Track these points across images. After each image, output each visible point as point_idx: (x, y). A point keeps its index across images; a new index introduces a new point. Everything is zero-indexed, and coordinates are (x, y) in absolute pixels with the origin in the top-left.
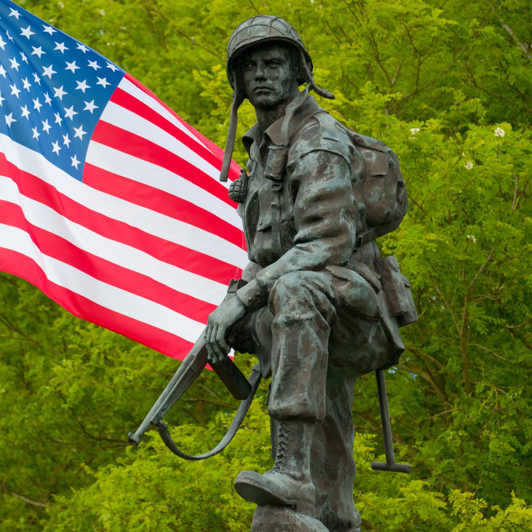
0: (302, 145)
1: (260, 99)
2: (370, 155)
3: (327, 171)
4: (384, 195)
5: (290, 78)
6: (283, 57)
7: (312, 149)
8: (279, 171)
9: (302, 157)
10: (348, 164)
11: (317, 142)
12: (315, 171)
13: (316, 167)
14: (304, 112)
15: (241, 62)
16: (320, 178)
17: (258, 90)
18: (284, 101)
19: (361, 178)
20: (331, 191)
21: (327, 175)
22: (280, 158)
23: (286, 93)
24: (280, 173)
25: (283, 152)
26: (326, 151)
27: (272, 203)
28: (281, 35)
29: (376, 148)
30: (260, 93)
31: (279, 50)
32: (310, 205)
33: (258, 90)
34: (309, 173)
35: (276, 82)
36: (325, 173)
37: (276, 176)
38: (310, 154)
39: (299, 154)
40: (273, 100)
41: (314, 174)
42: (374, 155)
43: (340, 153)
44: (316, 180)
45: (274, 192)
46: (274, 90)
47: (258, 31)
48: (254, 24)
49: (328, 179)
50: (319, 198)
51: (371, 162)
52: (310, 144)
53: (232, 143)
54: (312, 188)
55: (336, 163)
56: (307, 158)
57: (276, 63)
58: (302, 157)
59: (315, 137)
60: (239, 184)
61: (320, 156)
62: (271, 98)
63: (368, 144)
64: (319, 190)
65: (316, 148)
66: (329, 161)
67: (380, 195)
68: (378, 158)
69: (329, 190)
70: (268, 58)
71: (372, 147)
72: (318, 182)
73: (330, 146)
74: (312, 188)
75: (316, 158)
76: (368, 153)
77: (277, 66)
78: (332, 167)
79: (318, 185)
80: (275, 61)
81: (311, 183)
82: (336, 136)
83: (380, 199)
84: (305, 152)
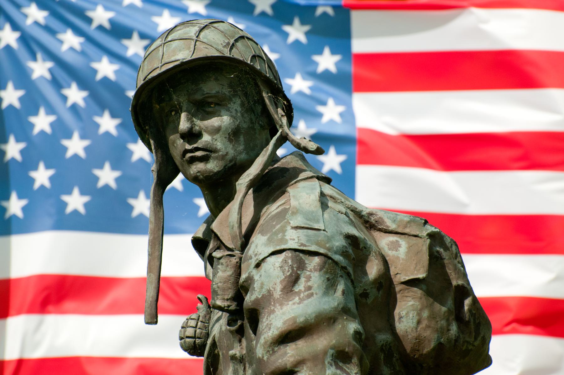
0: (259, 245)
1: (197, 168)
2: (395, 246)
3: (301, 286)
4: (426, 314)
5: (245, 126)
6: (226, 91)
7: (272, 250)
8: (230, 294)
9: (258, 266)
10: (344, 268)
11: (280, 236)
12: (279, 287)
13: (278, 281)
14: (275, 183)
15: (158, 105)
16: (288, 300)
17: (189, 155)
18: (236, 169)
19: (378, 290)
20: (306, 320)
21: (300, 291)
22: (230, 272)
23: (241, 153)
24: (233, 299)
25: (234, 260)
26: (296, 250)
27: (231, 352)
28: (217, 54)
29: (407, 231)
30: (193, 160)
31: (216, 79)
32: (274, 352)
33: (189, 155)
34: (270, 293)
35: (217, 136)
36: (296, 289)
37: (226, 304)
38: (269, 259)
39: (253, 262)
40: (216, 170)
41: (277, 293)
42: (403, 243)
43: (322, 251)
44: (281, 305)
45: (231, 332)
46: (215, 151)
47: (174, 52)
48: (169, 38)
49: (301, 300)
50: (288, 337)
51: (398, 258)
52: (270, 241)
53: (157, 254)
54: (275, 322)
55: (315, 270)
56: (264, 265)
57: (217, 104)
58: (258, 266)
59: (278, 227)
60: (193, 323)
61: (285, 261)
62: (213, 166)
63: (392, 226)
64: (284, 323)
65: (278, 248)
66: (301, 266)
67: (419, 314)
68: (410, 248)
69: (302, 319)
70: (198, 97)
71: (400, 230)
72: (285, 308)
73: (303, 241)
74: (275, 322)
75: (278, 265)
76: (392, 242)
77: (217, 108)
78: (309, 278)
79: (284, 314)
80: (210, 100)
81: (273, 312)
82: (318, 221)
83: (419, 322)
84: (261, 257)
